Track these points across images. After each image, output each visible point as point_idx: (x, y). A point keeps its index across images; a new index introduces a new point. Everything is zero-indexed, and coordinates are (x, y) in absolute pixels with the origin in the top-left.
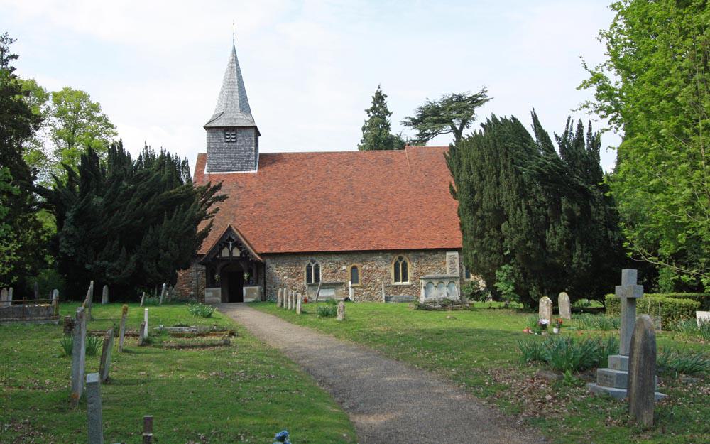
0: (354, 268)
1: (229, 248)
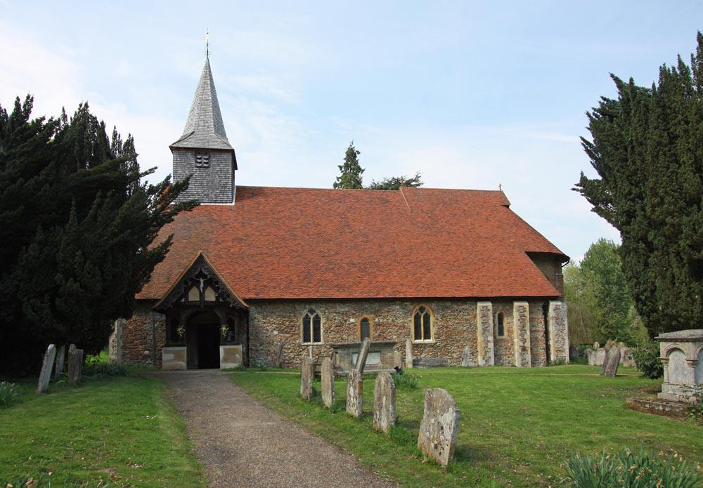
0: (365, 321)
1: (198, 288)
